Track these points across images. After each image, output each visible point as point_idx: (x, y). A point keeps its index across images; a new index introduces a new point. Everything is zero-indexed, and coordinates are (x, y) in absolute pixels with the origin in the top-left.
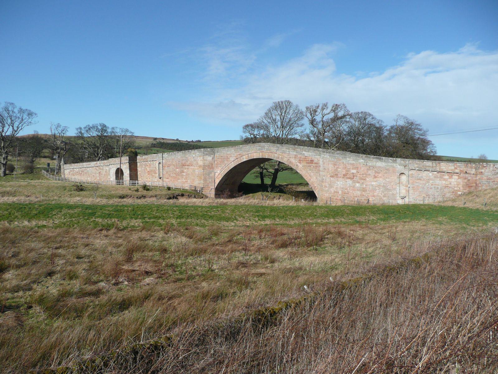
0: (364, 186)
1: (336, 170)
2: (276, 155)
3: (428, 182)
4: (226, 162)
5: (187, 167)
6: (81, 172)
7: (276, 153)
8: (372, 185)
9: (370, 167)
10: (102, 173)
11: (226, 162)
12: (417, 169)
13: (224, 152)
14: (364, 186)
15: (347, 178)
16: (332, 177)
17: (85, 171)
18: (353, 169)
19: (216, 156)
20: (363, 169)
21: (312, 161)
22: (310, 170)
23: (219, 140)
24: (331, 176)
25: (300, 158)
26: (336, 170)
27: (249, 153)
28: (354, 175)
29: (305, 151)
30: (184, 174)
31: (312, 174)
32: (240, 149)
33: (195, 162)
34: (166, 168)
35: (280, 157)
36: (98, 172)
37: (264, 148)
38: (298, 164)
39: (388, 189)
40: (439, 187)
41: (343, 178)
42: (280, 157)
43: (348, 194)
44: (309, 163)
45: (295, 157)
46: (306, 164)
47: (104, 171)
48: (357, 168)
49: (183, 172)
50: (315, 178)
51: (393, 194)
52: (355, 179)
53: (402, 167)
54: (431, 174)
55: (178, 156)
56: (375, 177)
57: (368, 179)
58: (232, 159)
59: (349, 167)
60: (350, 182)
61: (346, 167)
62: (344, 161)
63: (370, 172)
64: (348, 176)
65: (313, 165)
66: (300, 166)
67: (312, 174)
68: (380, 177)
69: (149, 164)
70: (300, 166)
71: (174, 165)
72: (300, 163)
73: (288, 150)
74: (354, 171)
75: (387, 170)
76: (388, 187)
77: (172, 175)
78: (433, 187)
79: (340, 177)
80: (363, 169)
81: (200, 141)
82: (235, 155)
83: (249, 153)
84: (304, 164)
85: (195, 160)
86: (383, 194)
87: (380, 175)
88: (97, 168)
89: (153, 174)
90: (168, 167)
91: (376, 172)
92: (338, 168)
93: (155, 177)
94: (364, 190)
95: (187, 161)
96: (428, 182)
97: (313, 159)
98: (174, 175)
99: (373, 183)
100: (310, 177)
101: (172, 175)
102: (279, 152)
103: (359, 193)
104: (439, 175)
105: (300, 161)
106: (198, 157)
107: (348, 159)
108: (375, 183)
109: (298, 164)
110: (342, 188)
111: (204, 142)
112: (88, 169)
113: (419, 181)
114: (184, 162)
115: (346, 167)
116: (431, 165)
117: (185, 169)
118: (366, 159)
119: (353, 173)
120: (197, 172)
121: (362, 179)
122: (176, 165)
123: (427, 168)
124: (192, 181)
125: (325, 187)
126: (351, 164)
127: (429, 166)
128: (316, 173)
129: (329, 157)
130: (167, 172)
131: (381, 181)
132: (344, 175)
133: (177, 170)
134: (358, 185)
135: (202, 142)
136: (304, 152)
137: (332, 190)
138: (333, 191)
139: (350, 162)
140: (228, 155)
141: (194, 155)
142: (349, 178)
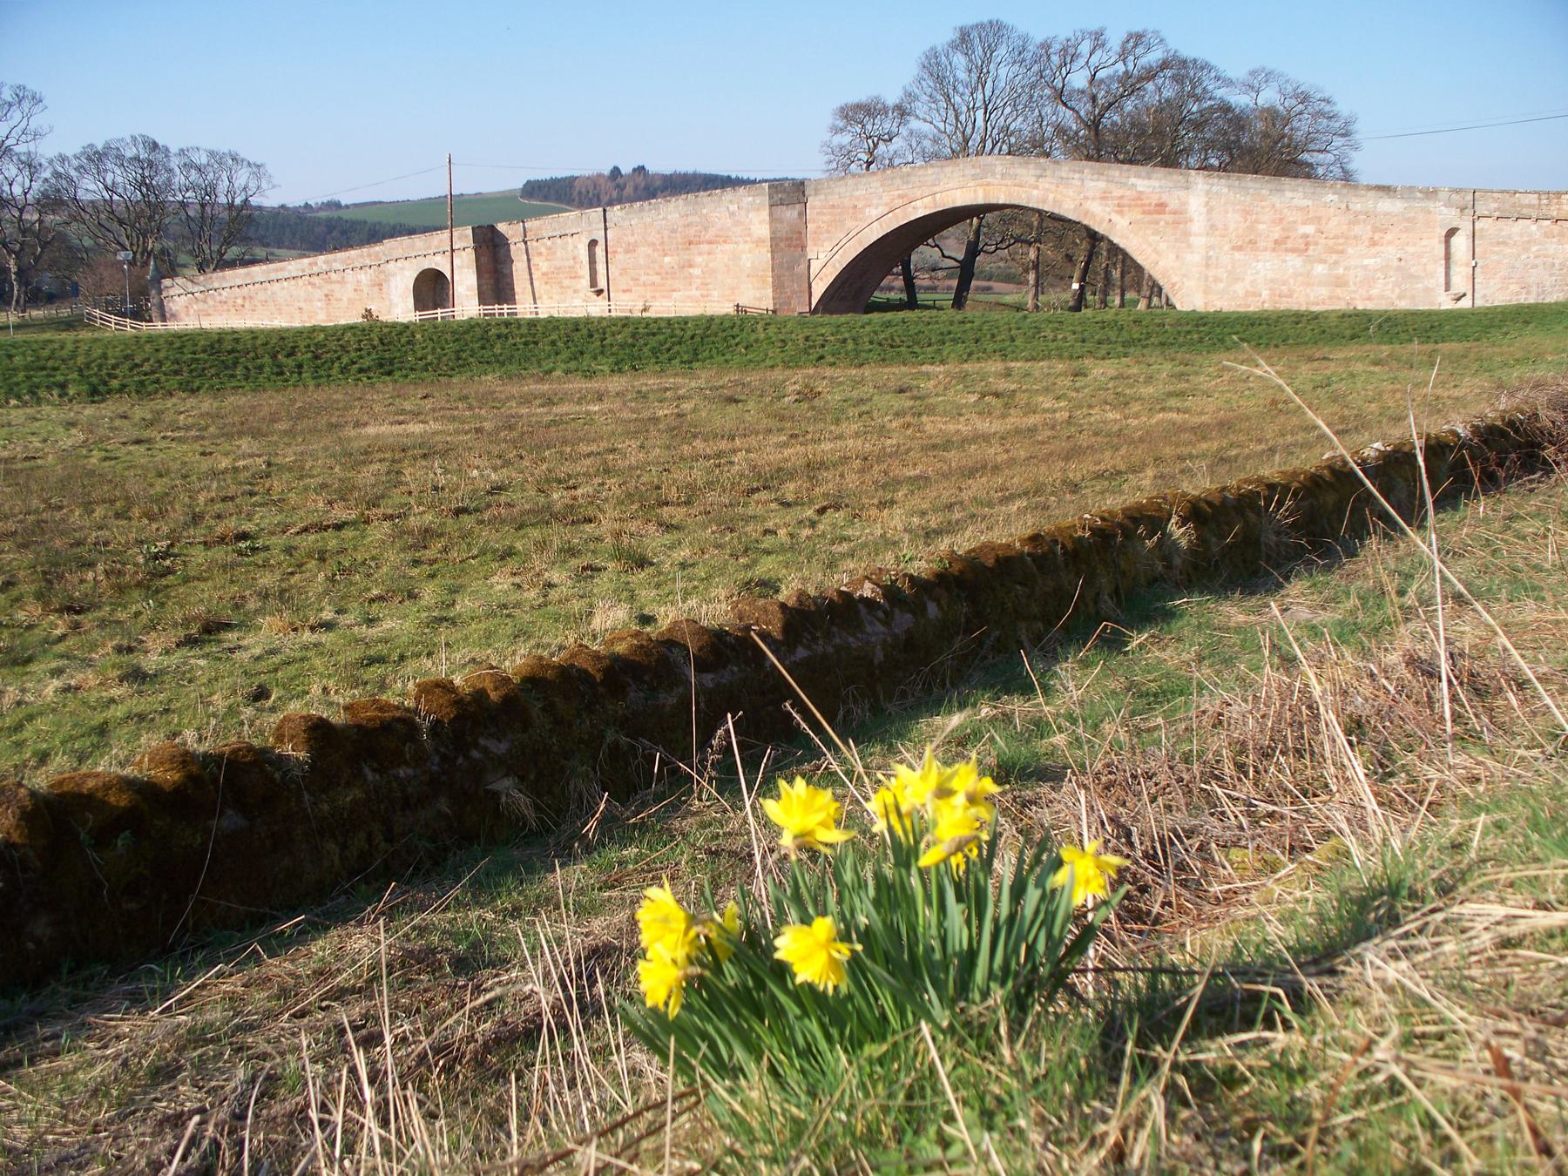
0: (1341, 271)
1: (1251, 228)
2: (1035, 192)
3: (1526, 250)
4: (850, 224)
5: (705, 247)
6: (240, 301)
7: (1037, 187)
8: (1365, 268)
9: (1356, 214)
10: (337, 295)
11: (850, 224)
12: (1497, 214)
13: (842, 190)
14: (1341, 271)
15: (1287, 250)
16: (1240, 248)
17: (261, 296)
18: (1304, 223)
19: (813, 208)
20: (1335, 221)
21: (1161, 207)
22: (1156, 233)
23: (414, 197)
24: (1233, 248)
25: (1122, 197)
26: (1251, 228)
27: (937, 189)
28: (1307, 241)
29: (1138, 176)
30: (696, 271)
31: (1163, 246)
32: (902, 178)
33: (738, 230)
34: (620, 257)
35: (1051, 196)
36: (319, 294)
37: (994, 174)
38: (1114, 217)
39: (1411, 276)
40: (1557, 262)
41: (1274, 250)
42: (1051, 196)
43: (1290, 296)
44: (1150, 213)
45: (1105, 197)
46: (1139, 217)
47: (350, 287)
48: (1319, 218)
49: (690, 266)
50: (1172, 256)
51: (1426, 290)
52: (1310, 252)
53: (1454, 212)
54: (1534, 227)
55: (672, 211)
56: (1373, 243)
57: (1350, 251)
58: (874, 213)
59: (1291, 216)
60: (1294, 262)
61: (1281, 220)
62: (1275, 200)
63: (1358, 230)
64: (1289, 245)
65: (1168, 217)
66: (1121, 222)
67: (1163, 246)
68: (1390, 243)
69: (549, 249)
70: (1121, 222)
71: (653, 244)
72: (1121, 213)
73: (1077, 176)
74: (1310, 229)
75: (1408, 220)
76: (1413, 270)
77: (643, 278)
78: (1538, 261)
79: (1266, 250)
80: (1336, 224)
81: (338, 205)
82: (886, 198)
83: (937, 189)
84: (1136, 215)
85: (737, 223)
86: (1397, 291)
87: (1389, 237)
88: (315, 279)
89: (566, 282)
90: (627, 252)
91: (1375, 229)
92: (1257, 221)
93: (575, 291)
94: (1340, 282)
95: (706, 229)
96: (1526, 250)
97: (1165, 198)
98: (657, 279)
99: (1366, 262)
100: (1154, 256)
101: (643, 278)
102: (1044, 183)
103: (1324, 292)
104: (1556, 228)
105: (1120, 209)
106: (748, 211)
107: (1289, 194)
108: (1372, 261)
109: (1114, 217)
110: (1272, 281)
111: (355, 205)
112: (276, 286)
113: (1502, 247)
114: (692, 231)
115: (1281, 220)
116: (1536, 202)
117: (700, 254)
118: (1345, 191)
119: (1306, 236)
120: (747, 261)
121: (1332, 251)
122: (662, 243)
123: (1525, 211)
124: (728, 292)
125: (1217, 280)
126: (1299, 209)
127: (1530, 206)
128: (1177, 240)
129: (1225, 190)
130: (624, 271)
131: (1391, 252)
132: (1276, 242)
133: (667, 259)
134: (1320, 269)
135: (347, 207)
136: (1133, 180)
137: (1240, 289)
138: (1241, 293)
139: (1296, 202)
140: (858, 199)
141: (734, 207)
142: (1294, 250)
